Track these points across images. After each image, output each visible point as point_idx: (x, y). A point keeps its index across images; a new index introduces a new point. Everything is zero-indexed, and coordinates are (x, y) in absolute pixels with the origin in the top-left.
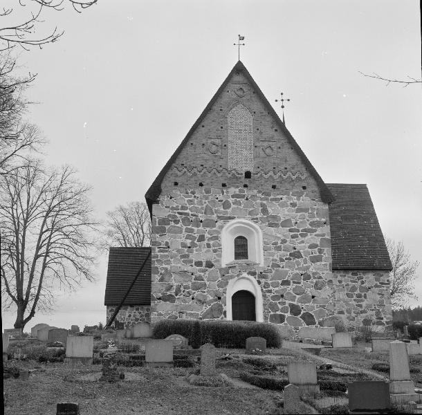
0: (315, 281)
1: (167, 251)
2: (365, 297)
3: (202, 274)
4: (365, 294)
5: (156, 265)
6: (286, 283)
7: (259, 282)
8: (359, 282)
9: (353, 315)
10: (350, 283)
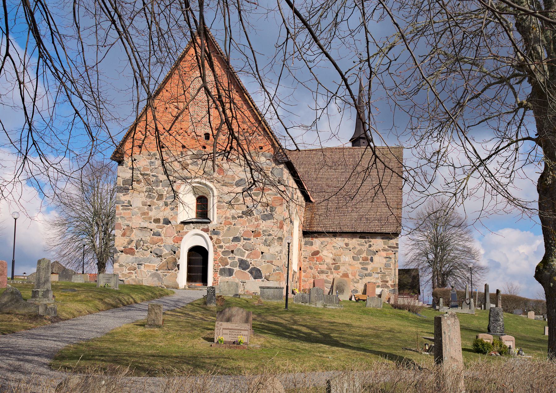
0: (264, 238)
1: (128, 209)
2: (372, 260)
3: (160, 230)
4: (372, 258)
5: (120, 221)
6: (236, 239)
7: (211, 238)
8: (367, 245)
9: (358, 278)
10: (357, 246)
